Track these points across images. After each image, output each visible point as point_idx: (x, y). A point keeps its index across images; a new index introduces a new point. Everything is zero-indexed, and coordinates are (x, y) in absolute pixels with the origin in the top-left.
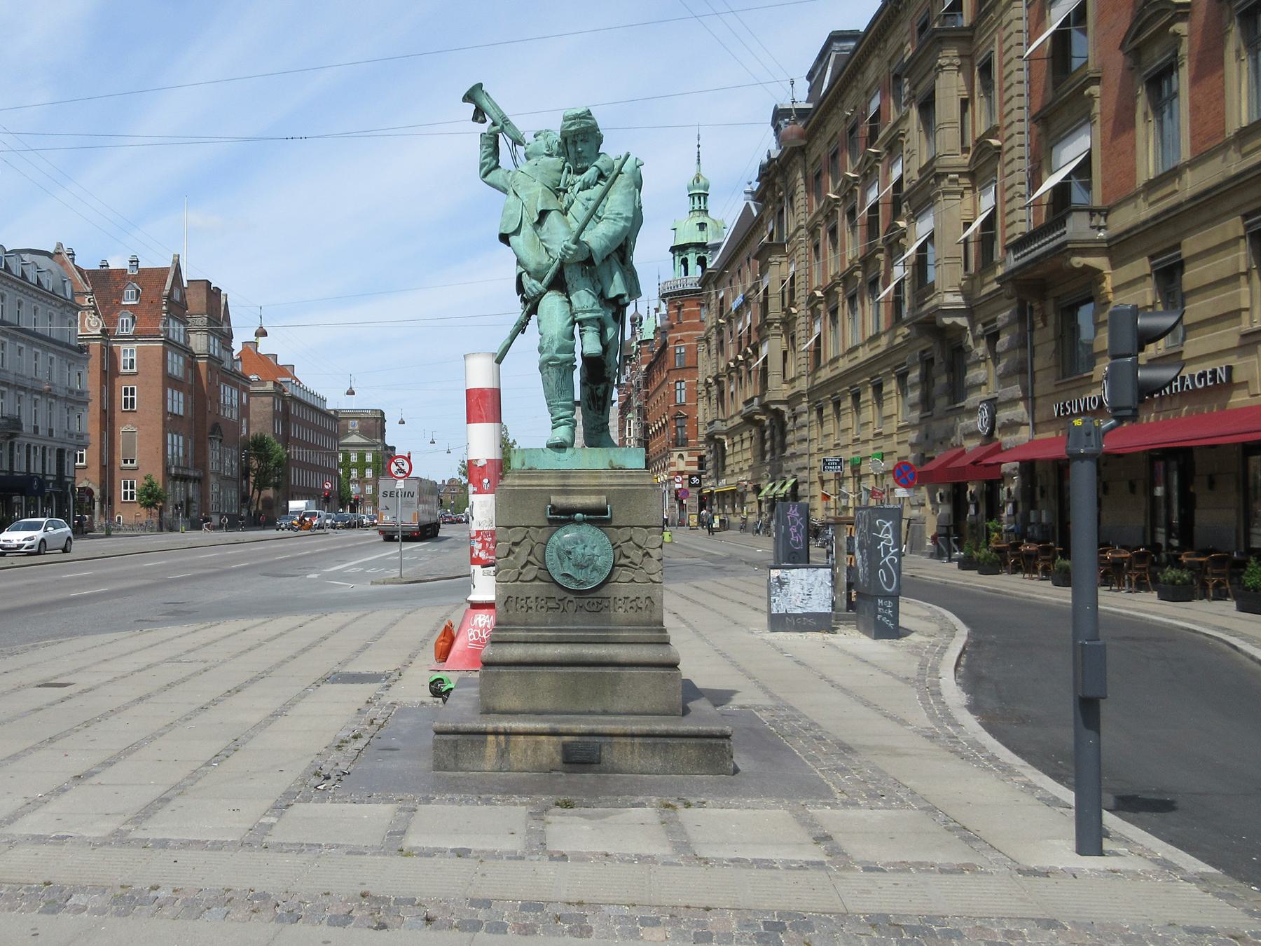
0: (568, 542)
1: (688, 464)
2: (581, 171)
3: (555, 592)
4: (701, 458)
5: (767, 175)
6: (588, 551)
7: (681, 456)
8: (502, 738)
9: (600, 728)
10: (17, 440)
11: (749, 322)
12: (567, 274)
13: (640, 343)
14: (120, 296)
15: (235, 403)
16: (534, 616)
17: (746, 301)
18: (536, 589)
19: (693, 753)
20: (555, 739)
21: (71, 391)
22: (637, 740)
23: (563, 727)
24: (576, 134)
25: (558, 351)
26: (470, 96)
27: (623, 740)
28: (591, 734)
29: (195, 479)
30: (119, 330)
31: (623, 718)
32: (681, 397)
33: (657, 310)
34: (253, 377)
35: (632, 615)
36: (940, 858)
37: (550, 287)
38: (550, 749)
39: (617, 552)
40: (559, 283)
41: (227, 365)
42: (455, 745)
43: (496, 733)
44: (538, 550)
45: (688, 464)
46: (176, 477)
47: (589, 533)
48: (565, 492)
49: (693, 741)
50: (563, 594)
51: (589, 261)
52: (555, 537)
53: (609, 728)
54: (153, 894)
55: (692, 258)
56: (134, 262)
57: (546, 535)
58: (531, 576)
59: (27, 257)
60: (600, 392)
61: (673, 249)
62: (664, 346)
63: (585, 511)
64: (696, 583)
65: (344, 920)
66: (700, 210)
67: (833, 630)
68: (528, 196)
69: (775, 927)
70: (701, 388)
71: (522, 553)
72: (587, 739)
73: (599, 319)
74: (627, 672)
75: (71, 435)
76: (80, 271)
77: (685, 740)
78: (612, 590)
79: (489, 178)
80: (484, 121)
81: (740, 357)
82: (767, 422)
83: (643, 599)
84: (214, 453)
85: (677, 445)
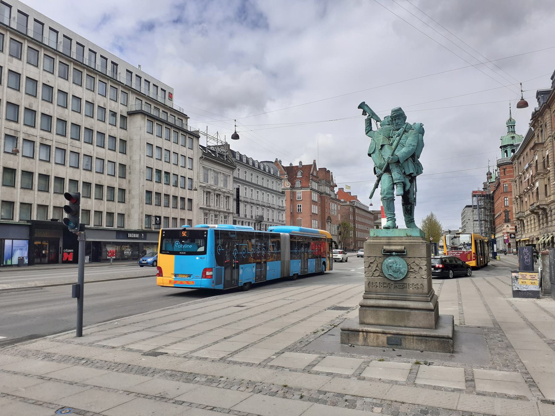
0: (390, 263)
1: (511, 229)
2: (398, 130)
3: (386, 281)
4: (516, 227)
6: (398, 266)
7: (508, 226)
8: (365, 333)
9: (401, 332)
10: (262, 223)
12: (391, 167)
14: (296, 175)
15: (336, 209)
16: (379, 289)
17: (530, 166)
19: (437, 344)
20: (384, 335)
21: (280, 207)
22: (415, 338)
26: (362, 106)
27: (410, 337)
31: (411, 329)
32: (507, 203)
34: (342, 200)
36: (512, 393)
37: (385, 172)
38: (383, 338)
39: (409, 267)
40: (388, 170)
41: (333, 196)
42: (348, 335)
43: (363, 332)
44: (379, 265)
45: (511, 229)
47: (398, 260)
48: (389, 244)
49: (436, 339)
50: (389, 282)
51: (398, 162)
53: (404, 332)
54: (221, 379)
55: (509, 150)
57: (382, 260)
58: (377, 275)
59: (265, 164)
60: (409, 208)
61: (501, 147)
62: (499, 184)
63: (396, 252)
64: (498, 277)
66: (512, 132)
67: (538, 298)
69: (424, 412)
70: (514, 200)
71: (374, 266)
72: (396, 336)
73: (402, 182)
75: (280, 221)
76: (283, 167)
77: (433, 339)
78: (408, 281)
81: (528, 188)
82: (540, 213)
83: (419, 285)
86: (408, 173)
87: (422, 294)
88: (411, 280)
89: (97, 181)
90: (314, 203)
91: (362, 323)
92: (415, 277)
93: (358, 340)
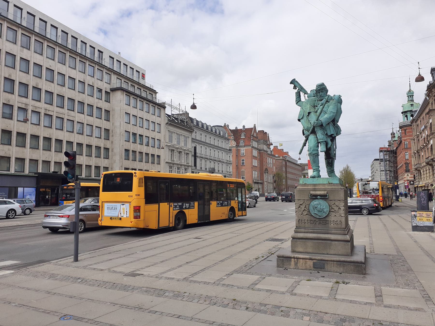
0: (316, 205)
1: (410, 177)
2: (321, 100)
3: (312, 218)
4: (414, 176)
5: (430, 89)
6: (322, 207)
7: (408, 175)
8: (296, 259)
9: (324, 258)
11: (427, 133)
12: (316, 130)
13: (393, 141)
14: (241, 136)
15: (271, 162)
16: (307, 225)
17: (426, 127)
18: (307, 218)
19: (352, 267)
20: (311, 261)
22: (335, 263)
23: (313, 257)
24: (319, 90)
25: (313, 151)
26: (293, 82)
27: (331, 262)
28: (321, 260)
29: (261, 183)
30: (241, 144)
33: (398, 131)
34: (277, 155)
35: (335, 226)
37: (311, 133)
38: (310, 263)
40: (313, 132)
41: (269, 153)
43: (294, 258)
44: (307, 206)
45: (410, 177)
46: (255, 183)
47: (322, 202)
48: (315, 190)
49: (352, 264)
51: (322, 125)
52: (312, 203)
53: (326, 259)
55: (409, 115)
56: (244, 126)
59: (216, 128)
61: (402, 113)
62: (401, 142)
63: (320, 196)
64: (399, 215)
65: (226, 306)
66: (411, 100)
68: (306, 109)
69: (343, 320)
70: (413, 154)
71: (303, 207)
73: (325, 141)
74: (334, 243)
75: (228, 172)
79: (298, 104)
80: (296, 89)
84: (265, 176)
85: (406, 172)
86: (329, 134)
87: (341, 228)
88: (332, 218)
89: (88, 142)
90: (255, 158)
91: (293, 251)
92: (335, 216)
93: (290, 265)
